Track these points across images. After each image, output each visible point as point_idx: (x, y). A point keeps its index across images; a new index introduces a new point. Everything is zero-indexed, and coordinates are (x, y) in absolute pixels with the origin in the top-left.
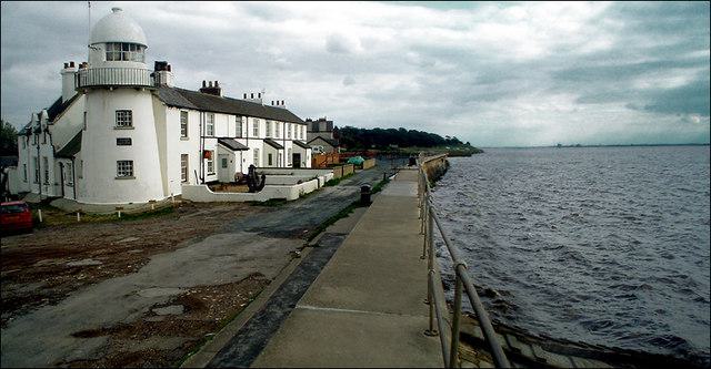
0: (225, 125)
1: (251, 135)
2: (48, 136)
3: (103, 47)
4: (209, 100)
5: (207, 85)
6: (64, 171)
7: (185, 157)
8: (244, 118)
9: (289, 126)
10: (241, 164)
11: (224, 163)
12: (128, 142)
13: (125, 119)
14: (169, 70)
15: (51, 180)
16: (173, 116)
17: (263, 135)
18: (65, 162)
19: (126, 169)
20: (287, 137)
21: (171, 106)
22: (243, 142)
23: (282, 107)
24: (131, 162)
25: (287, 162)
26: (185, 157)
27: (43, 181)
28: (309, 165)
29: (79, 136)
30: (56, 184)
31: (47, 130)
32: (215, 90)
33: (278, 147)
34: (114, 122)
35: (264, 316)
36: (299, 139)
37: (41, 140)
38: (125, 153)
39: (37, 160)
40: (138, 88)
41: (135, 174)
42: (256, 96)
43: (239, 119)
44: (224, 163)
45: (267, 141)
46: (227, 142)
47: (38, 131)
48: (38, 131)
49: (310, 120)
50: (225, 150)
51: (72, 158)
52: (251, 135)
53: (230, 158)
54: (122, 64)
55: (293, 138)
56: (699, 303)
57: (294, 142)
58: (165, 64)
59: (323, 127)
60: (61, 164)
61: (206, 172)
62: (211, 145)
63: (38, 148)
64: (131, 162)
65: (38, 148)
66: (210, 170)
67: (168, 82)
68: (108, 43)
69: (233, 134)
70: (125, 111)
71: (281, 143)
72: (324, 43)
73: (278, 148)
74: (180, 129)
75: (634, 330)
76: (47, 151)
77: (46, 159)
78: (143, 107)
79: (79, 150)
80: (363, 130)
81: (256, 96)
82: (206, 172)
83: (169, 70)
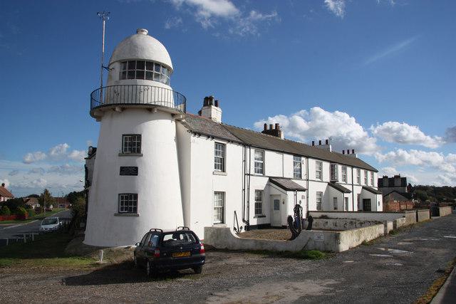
0: (279, 165)
5: (268, 128)
7: (221, 195)
8: (303, 159)
13: (133, 144)
19: (129, 204)
22: (302, 184)
25: (353, 205)
28: (380, 209)
33: (343, 190)
34: (118, 146)
35: (430, 235)
36: (370, 185)
46: (280, 181)
49: (386, 177)
50: (276, 190)
52: (355, 182)
56: (329, 249)
57: (363, 188)
59: (398, 183)
64: (136, 196)
71: (349, 188)
72: (43, 192)
73: (343, 192)
75: (387, 262)
80: (434, 187)
83: (216, 105)
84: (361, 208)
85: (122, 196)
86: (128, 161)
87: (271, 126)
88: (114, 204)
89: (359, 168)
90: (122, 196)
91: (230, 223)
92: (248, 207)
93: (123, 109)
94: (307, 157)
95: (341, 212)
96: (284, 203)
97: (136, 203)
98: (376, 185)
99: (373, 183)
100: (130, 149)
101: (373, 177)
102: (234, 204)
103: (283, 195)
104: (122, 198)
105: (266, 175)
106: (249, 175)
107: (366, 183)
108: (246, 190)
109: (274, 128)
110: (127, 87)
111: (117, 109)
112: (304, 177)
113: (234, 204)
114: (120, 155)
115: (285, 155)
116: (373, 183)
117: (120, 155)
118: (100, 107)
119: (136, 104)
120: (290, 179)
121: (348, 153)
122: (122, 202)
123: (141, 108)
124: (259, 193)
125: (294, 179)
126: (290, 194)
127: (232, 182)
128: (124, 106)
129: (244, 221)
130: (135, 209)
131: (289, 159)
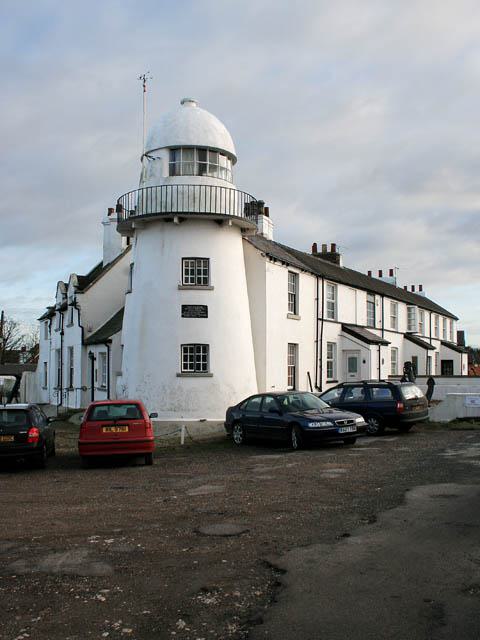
0: (352, 305)
1: (387, 326)
2: (76, 312)
3: (165, 155)
4: (325, 265)
5: (319, 250)
6: (96, 366)
7: (293, 347)
8: (378, 297)
9: (437, 318)
10: (380, 366)
11: (353, 364)
12: (200, 312)
13: (197, 272)
14: (267, 215)
15: (77, 383)
16: (277, 276)
17: (403, 327)
19: (196, 359)
20: (433, 336)
21: (273, 259)
22: (378, 333)
23: (419, 293)
24: (206, 348)
26: (293, 347)
27: (65, 384)
29: (123, 309)
30: (83, 389)
31: (74, 304)
32: (332, 256)
34: (176, 274)
36: (448, 340)
37: (66, 323)
38: (195, 331)
39: (60, 352)
40: (220, 221)
41: (213, 281)
42: (386, 274)
43: (371, 298)
44: (353, 364)
45: (408, 336)
46: (357, 330)
47: (63, 308)
48: (63, 308)
50: (352, 343)
51: (107, 342)
53: (363, 355)
54: (205, 180)
55: (441, 338)
58: (261, 204)
61: (325, 378)
62: (332, 332)
63: (62, 334)
64: (206, 348)
65: (62, 334)
66: (330, 374)
67: (265, 231)
68: (174, 150)
69: (362, 321)
70: (198, 259)
71: (428, 341)
72: (211, 372)
74: (285, 300)
76: (74, 337)
77: (71, 349)
78: (227, 253)
79: (121, 328)
81: (386, 274)
82: (325, 378)
83: (267, 215)
84: (439, 374)
85: (185, 348)
86: (195, 297)
87: (324, 246)
88: (176, 361)
89: (431, 311)
90: (185, 348)
91: (303, 386)
92: (321, 367)
93: (181, 220)
94: (382, 295)
95: (458, 377)
96: (364, 362)
97: (205, 358)
98: (455, 341)
99: (451, 337)
100: (192, 280)
101: (451, 328)
102: (306, 363)
103: (363, 351)
104: (185, 350)
105: (340, 326)
106: (322, 320)
107: (444, 336)
108: (318, 341)
109: (329, 250)
110: (186, 188)
111: (176, 220)
112: (378, 326)
113: (306, 363)
114: (180, 288)
115: (358, 291)
116: (451, 337)
117: (180, 288)
118: (143, 216)
119: (205, 213)
120: (363, 327)
121: (413, 290)
122: (185, 357)
123: (159, 220)
124: (331, 345)
125: (368, 327)
126: (373, 348)
127: (303, 330)
128: (147, 219)
129: (316, 387)
130: (205, 367)
131: (362, 295)
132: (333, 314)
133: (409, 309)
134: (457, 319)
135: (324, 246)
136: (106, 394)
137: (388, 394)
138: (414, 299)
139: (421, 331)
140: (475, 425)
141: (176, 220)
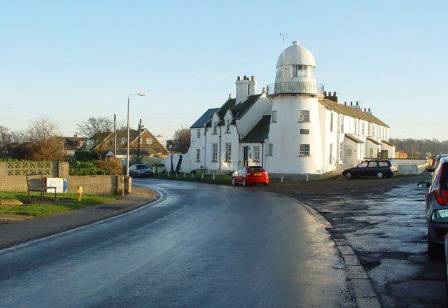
0: (350, 124)
1: (361, 134)
5: (328, 95)
17: (366, 135)
18: (251, 145)
24: (308, 146)
50: (350, 142)
52: (361, 134)
60: (246, 149)
63: (220, 136)
64: (308, 146)
77: (229, 146)
87: (330, 93)
88: (298, 151)
97: (308, 150)
109: (332, 95)
112: (357, 133)
132: (342, 130)
133: (369, 124)
134: (388, 127)
135: (330, 93)
136: (29, 179)
137: (386, 164)
138: (368, 116)
139: (374, 136)
140: (11, 254)
141: (380, 175)
